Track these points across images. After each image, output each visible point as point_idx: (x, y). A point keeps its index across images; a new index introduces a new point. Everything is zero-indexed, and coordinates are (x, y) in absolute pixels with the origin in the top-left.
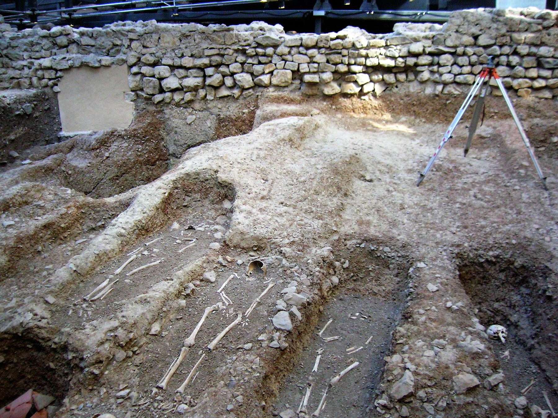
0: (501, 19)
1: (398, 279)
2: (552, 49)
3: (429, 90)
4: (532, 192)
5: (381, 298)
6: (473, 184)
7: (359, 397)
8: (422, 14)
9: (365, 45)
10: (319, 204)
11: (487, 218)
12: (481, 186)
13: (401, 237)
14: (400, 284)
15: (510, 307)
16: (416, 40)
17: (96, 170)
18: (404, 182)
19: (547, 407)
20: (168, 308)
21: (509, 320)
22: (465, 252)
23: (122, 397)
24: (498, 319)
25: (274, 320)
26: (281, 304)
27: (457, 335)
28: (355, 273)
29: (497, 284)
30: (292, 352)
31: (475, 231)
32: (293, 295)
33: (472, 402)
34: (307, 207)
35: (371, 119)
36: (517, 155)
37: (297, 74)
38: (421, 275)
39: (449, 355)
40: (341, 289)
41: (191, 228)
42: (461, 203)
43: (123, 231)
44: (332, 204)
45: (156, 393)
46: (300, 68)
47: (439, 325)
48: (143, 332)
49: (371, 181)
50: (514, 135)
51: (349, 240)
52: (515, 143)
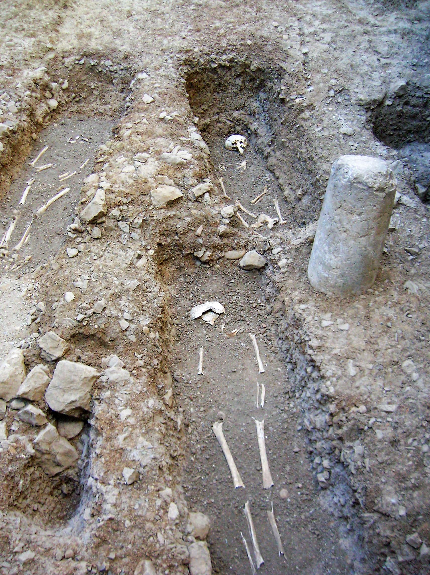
10: (31, 20)
11: (223, 18)
13: (124, 47)
22: (194, 58)
31: (208, 34)
33: (174, 215)
39: (149, 169)
44: (46, 18)
47: (148, 138)
51: (67, 57)
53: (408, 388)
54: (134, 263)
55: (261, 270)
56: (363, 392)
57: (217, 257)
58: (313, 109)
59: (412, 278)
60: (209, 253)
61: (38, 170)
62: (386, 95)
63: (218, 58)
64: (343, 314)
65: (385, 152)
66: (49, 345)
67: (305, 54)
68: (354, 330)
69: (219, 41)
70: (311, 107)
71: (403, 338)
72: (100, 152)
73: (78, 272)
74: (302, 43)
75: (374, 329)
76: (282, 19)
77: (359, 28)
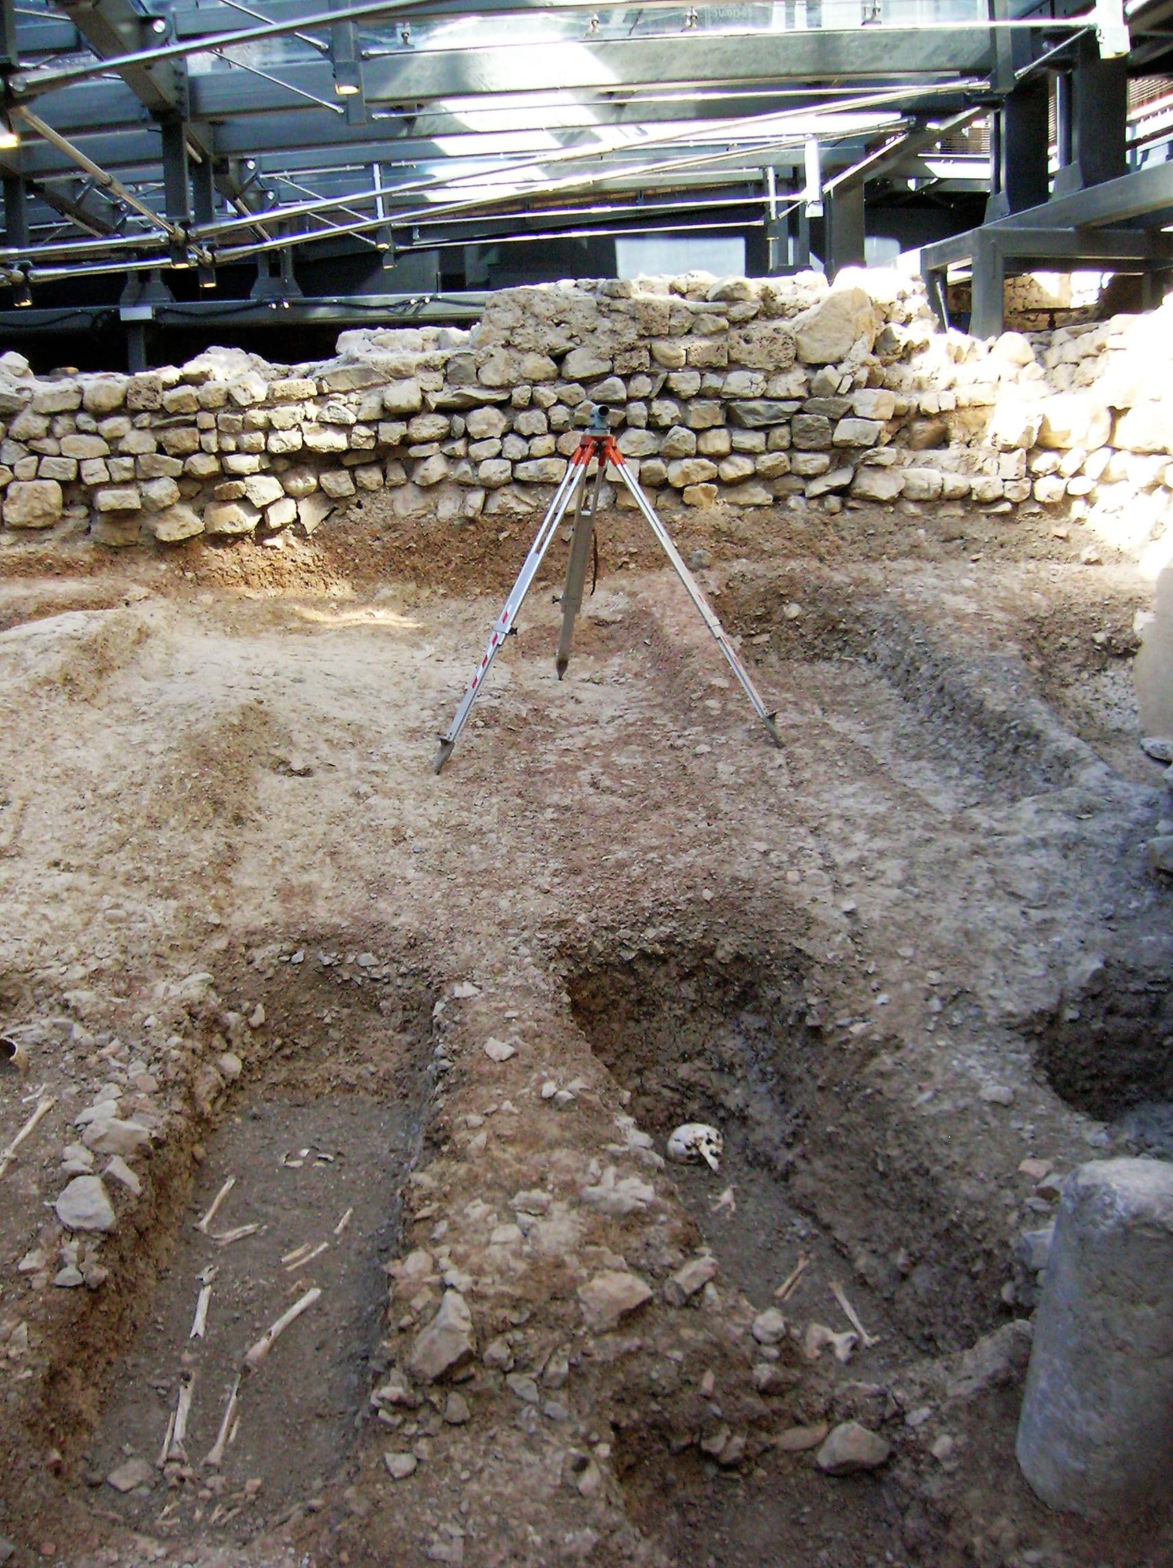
0: (620, 305)
1: (408, 1038)
2: (759, 377)
3: (448, 508)
4: (741, 755)
5: (368, 1098)
6: (587, 752)
7: (330, 1388)
8: (422, 301)
9: (261, 395)
10: (163, 855)
12: (607, 755)
13: (402, 919)
14: (416, 1051)
15: (721, 1070)
16: (400, 375)
18: (399, 766)
19: (848, 1325)
21: (722, 1105)
22: (580, 940)
24: (694, 1106)
25: (60, 1205)
26: (77, 1157)
27: (578, 1170)
28: (286, 1037)
29: (678, 1012)
30: (125, 1291)
32: (111, 1126)
33: (640, 1348)
34: (131, 866)
35: (297, 600)
36: (695, 663)
37: (76, 490)
38: (468, 1019)
39: (559, 1230)
40: (251, 1086)
42: (557, 807)
44: (200, 850)
46: (84, 472)
49: (306, 773)
50: (685, 609)
51: (258, 946)
52: (688, 630)
54: (571, 1482)
57: (759, 1448)
58: (898, 1048)
61: (222, 1243)
62: (1062, 995)
65: (1103, 1136)
67: (849, 914)
69: (632, 894)
70: (892, 1042)
73: (428, 1517)
74: (838, 888)
77: (958, 842)
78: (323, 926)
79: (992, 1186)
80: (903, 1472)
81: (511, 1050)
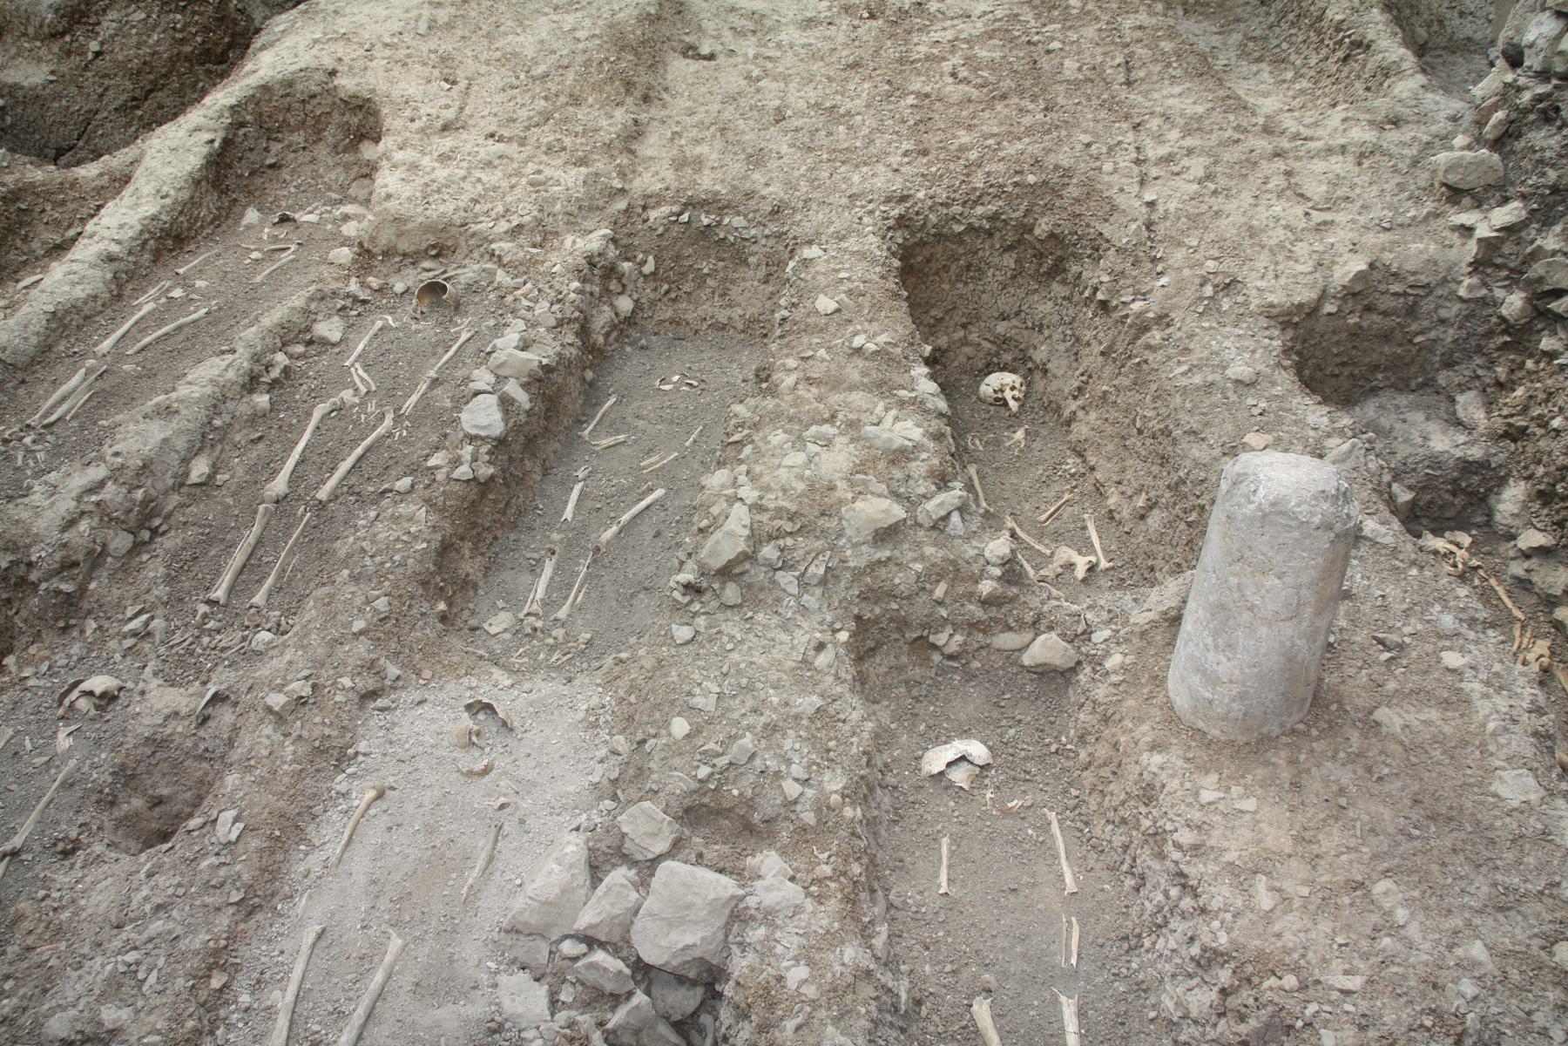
10: (580, 129)
12: (971, 48)
13: (771, 189)
17: (74, 90)
20: (227, 418)
23: (134, 634)
24: (1007, 357)
26: (482, 378)
31: (944, 161)
32: (510, 355)
33: (889, 559)
39: (837, 460)
41: (284, 219)
42: (918, 94)
43: (115, 248)
45: (205, 616)
48: (170, 482)
49: (711, 57)
53: (1386, 941)
55: (1068, 675)
56: (1290, 945)
57: (976, 646)
58: (1168, 325)
59: (1389, 700)
60: (958, 638)
63: (967, 211)
64: (1243, 777)
65: (1325, 420)
66: (642, 830)
68: (1267, 812)
69: (968, 175)
70: (1163, 320)
71: (1372, 830)
72: (733, 421)
73: (696, 676)
75: (1311, 811)
76: (1100, 126)
77: (1263, 144)
78: (706, 192)
79: (1217, 452)
80: (1083, 677)
81: (836, 306)
